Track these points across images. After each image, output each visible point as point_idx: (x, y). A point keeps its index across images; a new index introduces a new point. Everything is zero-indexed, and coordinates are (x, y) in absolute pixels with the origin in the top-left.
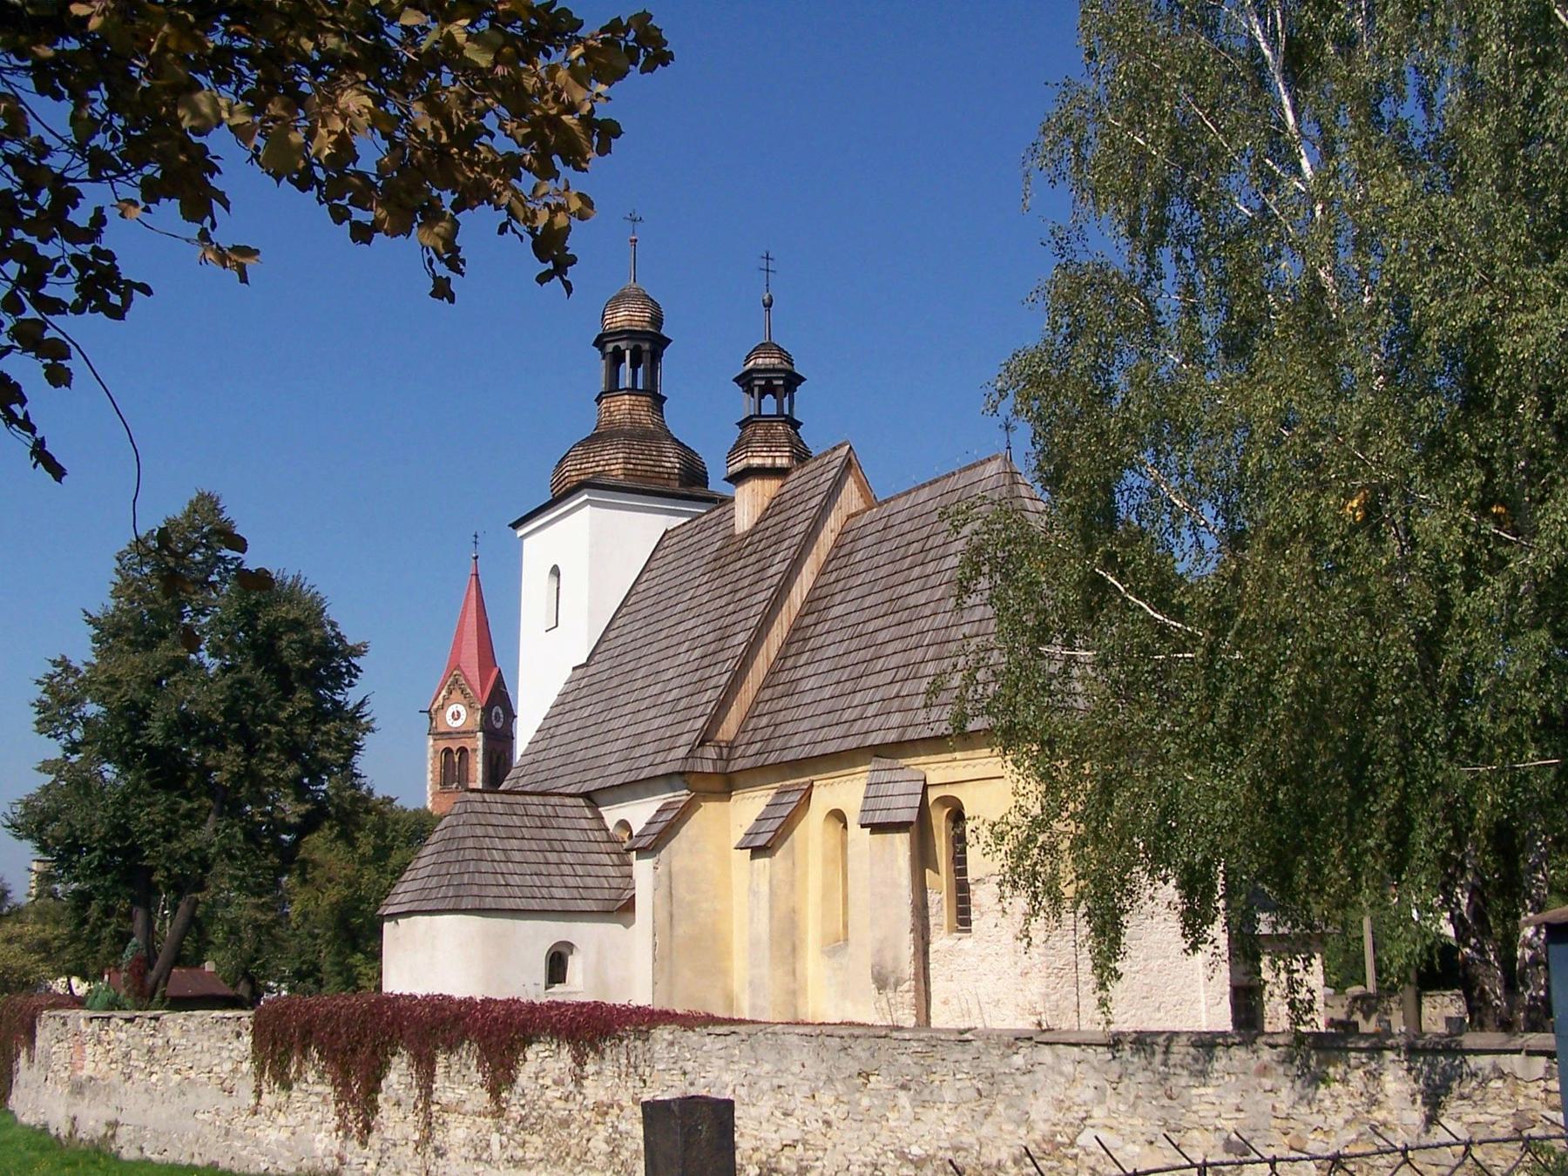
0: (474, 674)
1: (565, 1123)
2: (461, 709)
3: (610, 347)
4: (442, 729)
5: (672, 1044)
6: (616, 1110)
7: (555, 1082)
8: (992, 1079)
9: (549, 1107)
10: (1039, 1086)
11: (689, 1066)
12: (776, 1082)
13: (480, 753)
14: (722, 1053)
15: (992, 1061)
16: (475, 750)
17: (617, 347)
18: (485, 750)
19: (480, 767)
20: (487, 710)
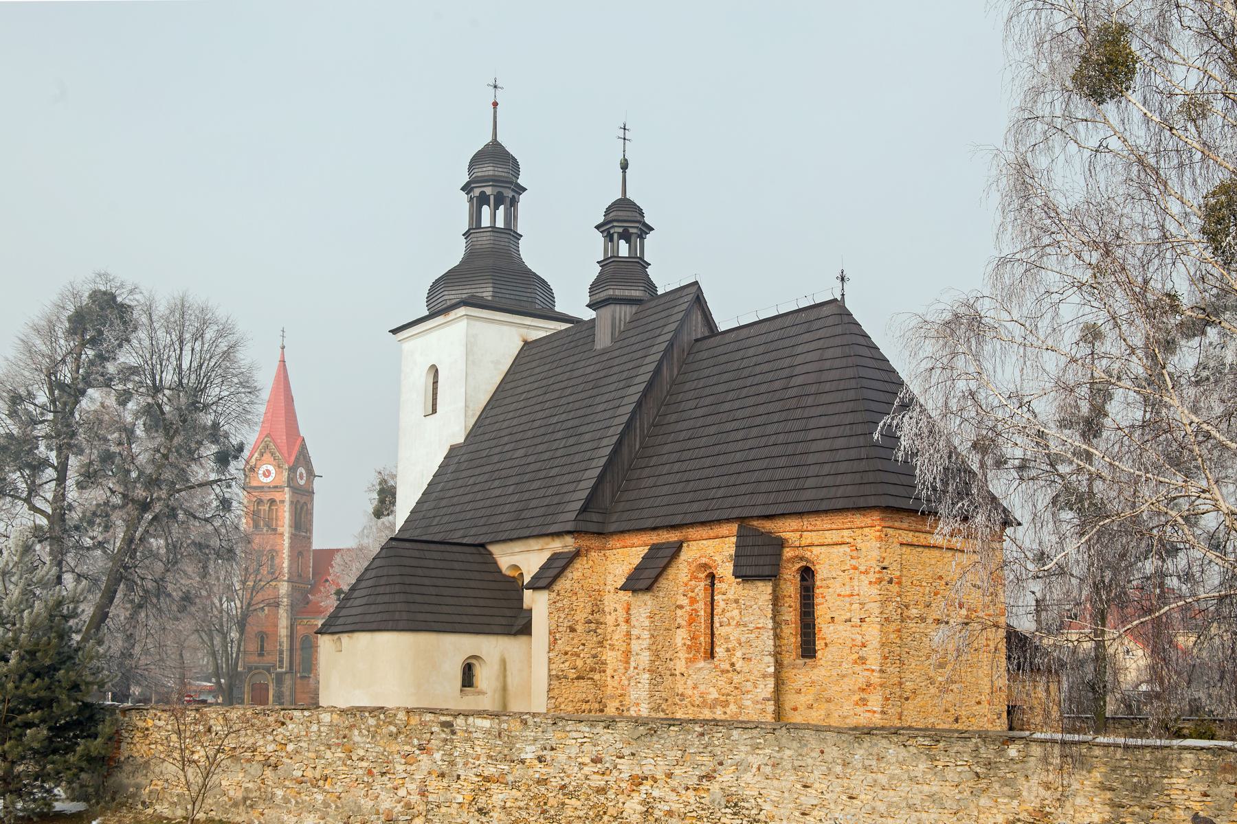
0: (282, 439)
1: (601, 791)
2: (271, 468)
3: (477, 192)
4: (254, 484)
5: (702, 734)
6: (650, 782)
7: (592, 761)
8: (989, 764)
9: (587, 778)
10: (1030, 773)
11: (718, 751)
12: (797, 763)
13: (287, 504)
14: (748, 742)
15: (987, 752)
16: (283, 502)
17: (483, 193)
18: (292, 502)
19: (287, 515)
20: (293, 470)
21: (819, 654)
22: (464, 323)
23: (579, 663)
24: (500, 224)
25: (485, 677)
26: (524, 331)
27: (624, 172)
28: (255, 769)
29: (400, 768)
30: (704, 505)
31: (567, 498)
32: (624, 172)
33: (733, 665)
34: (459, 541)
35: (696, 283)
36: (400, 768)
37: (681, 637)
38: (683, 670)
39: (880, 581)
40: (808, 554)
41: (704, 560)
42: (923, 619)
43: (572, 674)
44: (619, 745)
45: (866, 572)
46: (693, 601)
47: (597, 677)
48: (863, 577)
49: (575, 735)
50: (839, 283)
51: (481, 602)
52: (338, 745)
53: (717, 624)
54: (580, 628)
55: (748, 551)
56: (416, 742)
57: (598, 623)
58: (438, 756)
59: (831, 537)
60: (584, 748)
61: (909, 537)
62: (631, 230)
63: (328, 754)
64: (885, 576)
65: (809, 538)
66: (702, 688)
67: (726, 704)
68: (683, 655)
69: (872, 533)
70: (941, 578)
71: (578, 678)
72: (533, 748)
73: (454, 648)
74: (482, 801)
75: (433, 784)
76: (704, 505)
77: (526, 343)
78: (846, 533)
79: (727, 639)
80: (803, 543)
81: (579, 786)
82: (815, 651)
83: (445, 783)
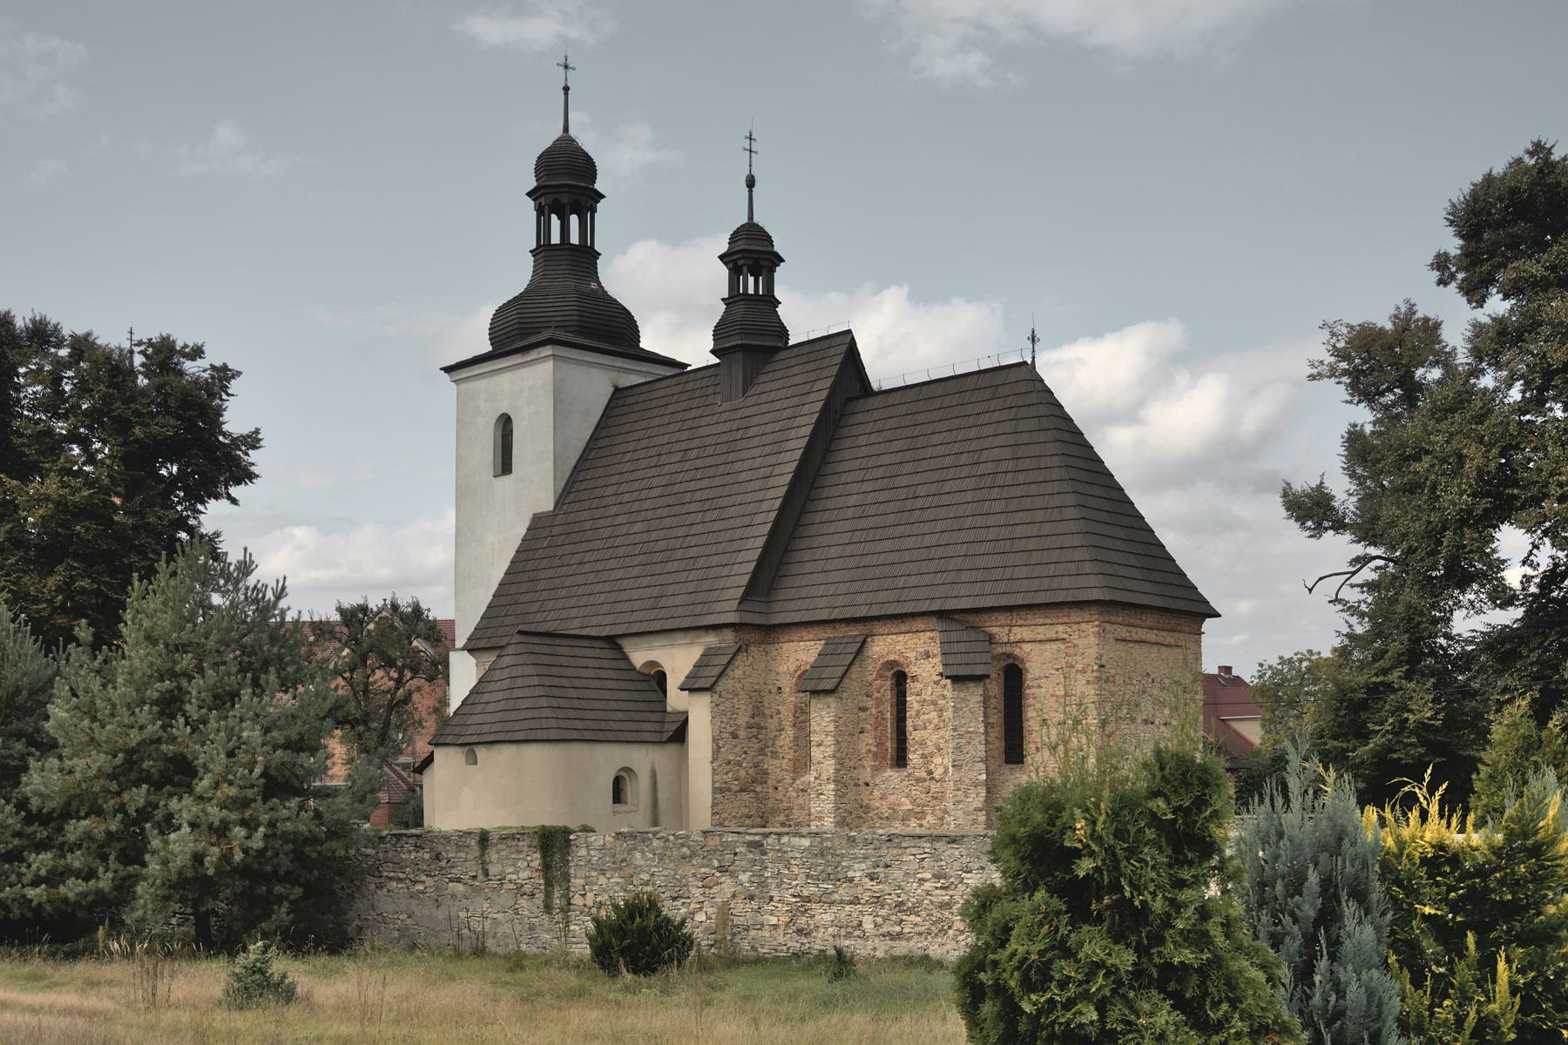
7: (934, 876)
21: (1028, 760)
22: (550, 365)
23: (742, 773)
24: (574, 239)
25: (639, 791)
26: (614, 374)
27: (751, 192)
28: (505, 899)
29: (696, 892)
30: (893, 595)
31: (721, 583)
32: (751, 192)
33: (930, 773)
34: (576, 632)
35: (849, 332)
36: (696, 892)
37: (867, 741)
38: (868, 779)
39: (1099, 679)
40: (1017, 651)
41: (892, 657)
42: (1133, 720)
43: (735, 786)
44: (964, 860)
45: (1084, 671)
46: (879, 702)
47: (759, 789)
48: (1079, 676)
49: (914, 851)
50: (1029, 343)
51: (623, 706)
52: (615, 870)
53: (909, 728)
54: (742, 734)
55: (955, 648)
56: (716, 864)
57: (760, 728)
58: (744, 877)
59: (1042, 632)
60: (925, 863)
61: (1123, 632)
62: (740, 263)
63: (602, 880)
64: (1103, 675)
65: (1019, 633)
66: (892, 798)
67: (920, 815)
68: (869, 763)
69: (1091, 629)
70: (1148, 675)
71: (741, 790)
72: (863, 866)
73: (607, 759)
74: (802, 921)
75: (739, 906)
76: (893, 595)
77: (617, 390)
78: (1061, 628)
79: (923, 744)
80: (1012, 638)
81: (920, 902)
82: (1023, 757)
83: (754, 905)
